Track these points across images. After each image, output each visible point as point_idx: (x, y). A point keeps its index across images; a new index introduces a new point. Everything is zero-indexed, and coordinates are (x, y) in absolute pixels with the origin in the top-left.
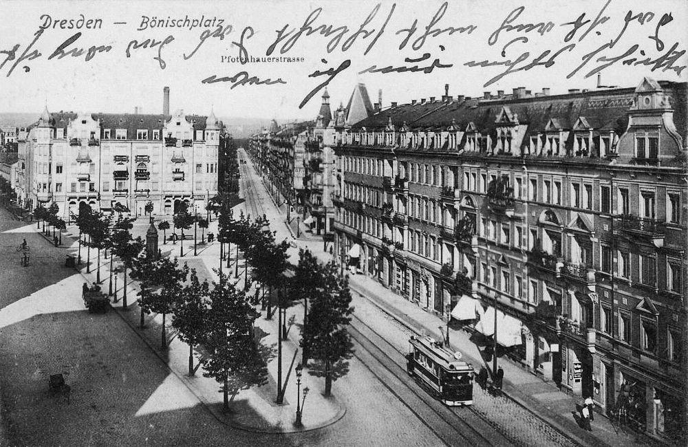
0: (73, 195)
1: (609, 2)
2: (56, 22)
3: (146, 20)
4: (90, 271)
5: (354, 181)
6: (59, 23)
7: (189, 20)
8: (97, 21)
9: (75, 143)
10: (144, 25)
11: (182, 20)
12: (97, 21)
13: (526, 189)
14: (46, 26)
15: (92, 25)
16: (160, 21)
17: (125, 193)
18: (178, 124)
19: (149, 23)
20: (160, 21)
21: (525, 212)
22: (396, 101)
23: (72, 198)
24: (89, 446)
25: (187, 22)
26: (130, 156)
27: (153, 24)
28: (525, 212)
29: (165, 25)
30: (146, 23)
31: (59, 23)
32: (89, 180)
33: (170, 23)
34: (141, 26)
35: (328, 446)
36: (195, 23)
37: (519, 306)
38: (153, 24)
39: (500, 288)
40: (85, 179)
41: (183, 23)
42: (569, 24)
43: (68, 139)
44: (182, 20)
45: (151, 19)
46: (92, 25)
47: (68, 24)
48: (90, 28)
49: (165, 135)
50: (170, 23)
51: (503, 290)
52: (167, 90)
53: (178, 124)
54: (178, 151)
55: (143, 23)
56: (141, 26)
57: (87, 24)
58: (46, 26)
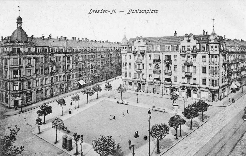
1: (161, 155)
3: (131, 10)
4: (41, 131)
6: (94, 11)
7: (146, 11)
8: (106, 11)
10: (130, 12)
11: (143, 11)
12: (106, 11)
14: (91, 13)
15: (105, 12)
16: (135, 11)
19: (132, 11)
20: (135, 11)
21: (17, 74)
25: (145, 11)
27: (133, 12)
28: (17, 74)
29: (137, 12)
30: (131, 11)
31: (94, 11)
33: (139, 12)
34: (129, 12)
36: (148, 11)
38: (133, 11)
41: (105, 12)
42: (56, 135)
44: (143, 11)
45: (132, 10)
46: (105, 12)
47: (98, 12)
48: (96, 13)
50: (139, 12)
55: (129, 11)
56: (129, 12)
58: (91, 13)
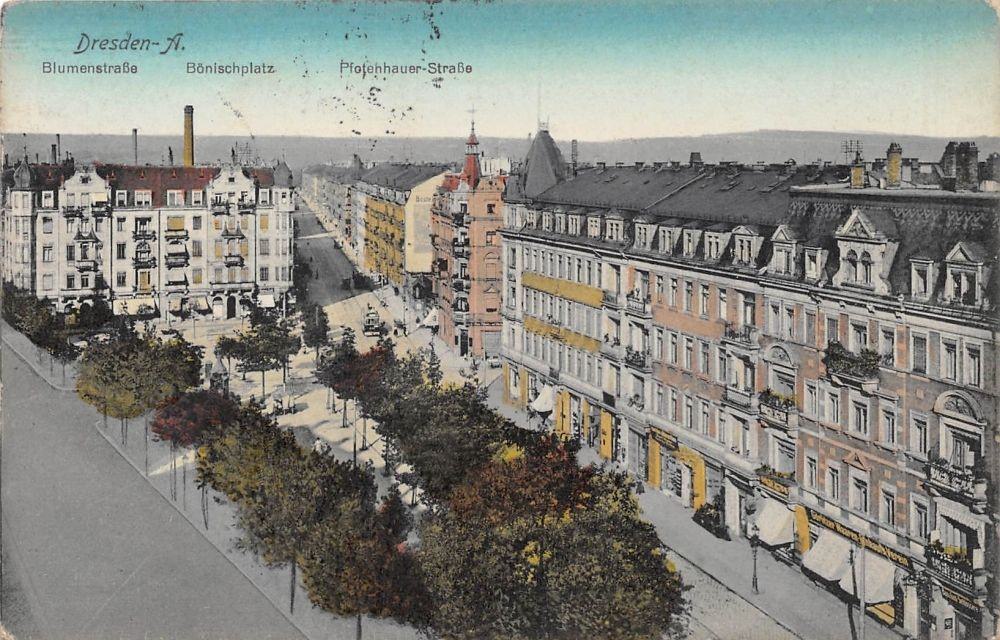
0: (71, 293)
2: (95, 41)
5: (896, 300)
6: (99, 43)
9: (71, 214)
13: (872, 293)
15: (138, 47)
17: (183, 287)
18: (232, 180)
22: (604, 161)
23: (218, 292)
24: (121, 639)
26: (157, 231)
31: (99, 43)
32: (96, 270)
35: (468, 638)
37: (890, 538)
39: (877, 518)
40: (88, 269)
43: (61, 210)
47: (110, 45)
49: (210, 195)
51: (828, 493)
52: (189, 110)
53: (232, 180)
54: (235, 219)
57: (132, 44)
